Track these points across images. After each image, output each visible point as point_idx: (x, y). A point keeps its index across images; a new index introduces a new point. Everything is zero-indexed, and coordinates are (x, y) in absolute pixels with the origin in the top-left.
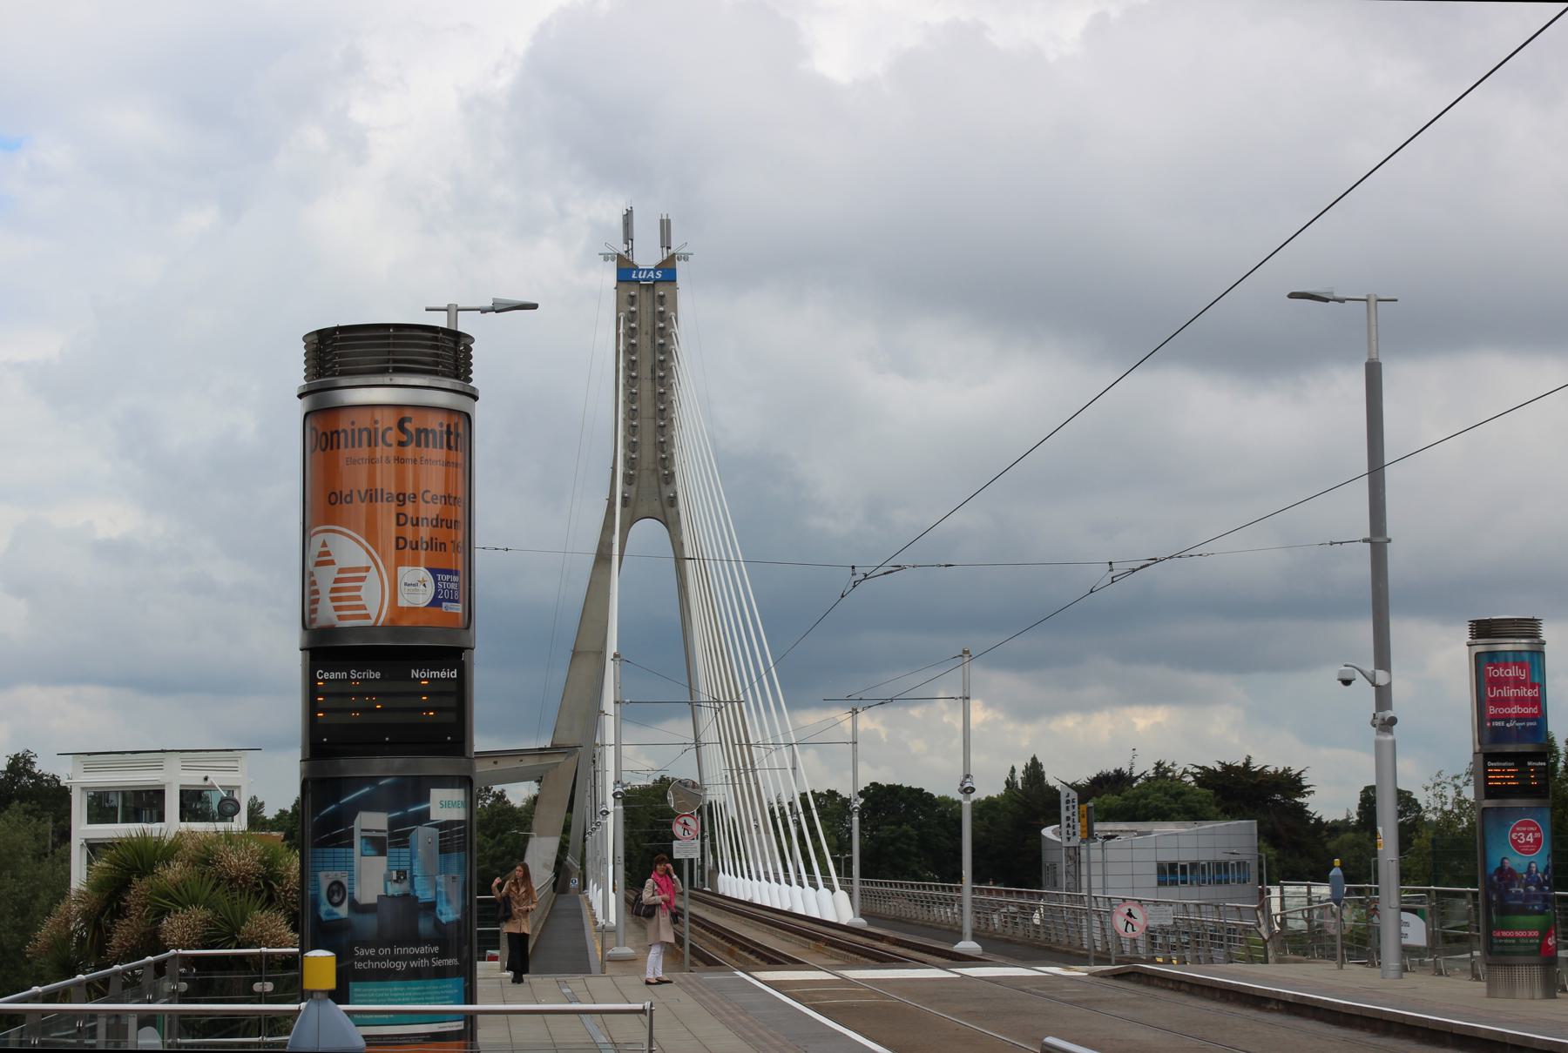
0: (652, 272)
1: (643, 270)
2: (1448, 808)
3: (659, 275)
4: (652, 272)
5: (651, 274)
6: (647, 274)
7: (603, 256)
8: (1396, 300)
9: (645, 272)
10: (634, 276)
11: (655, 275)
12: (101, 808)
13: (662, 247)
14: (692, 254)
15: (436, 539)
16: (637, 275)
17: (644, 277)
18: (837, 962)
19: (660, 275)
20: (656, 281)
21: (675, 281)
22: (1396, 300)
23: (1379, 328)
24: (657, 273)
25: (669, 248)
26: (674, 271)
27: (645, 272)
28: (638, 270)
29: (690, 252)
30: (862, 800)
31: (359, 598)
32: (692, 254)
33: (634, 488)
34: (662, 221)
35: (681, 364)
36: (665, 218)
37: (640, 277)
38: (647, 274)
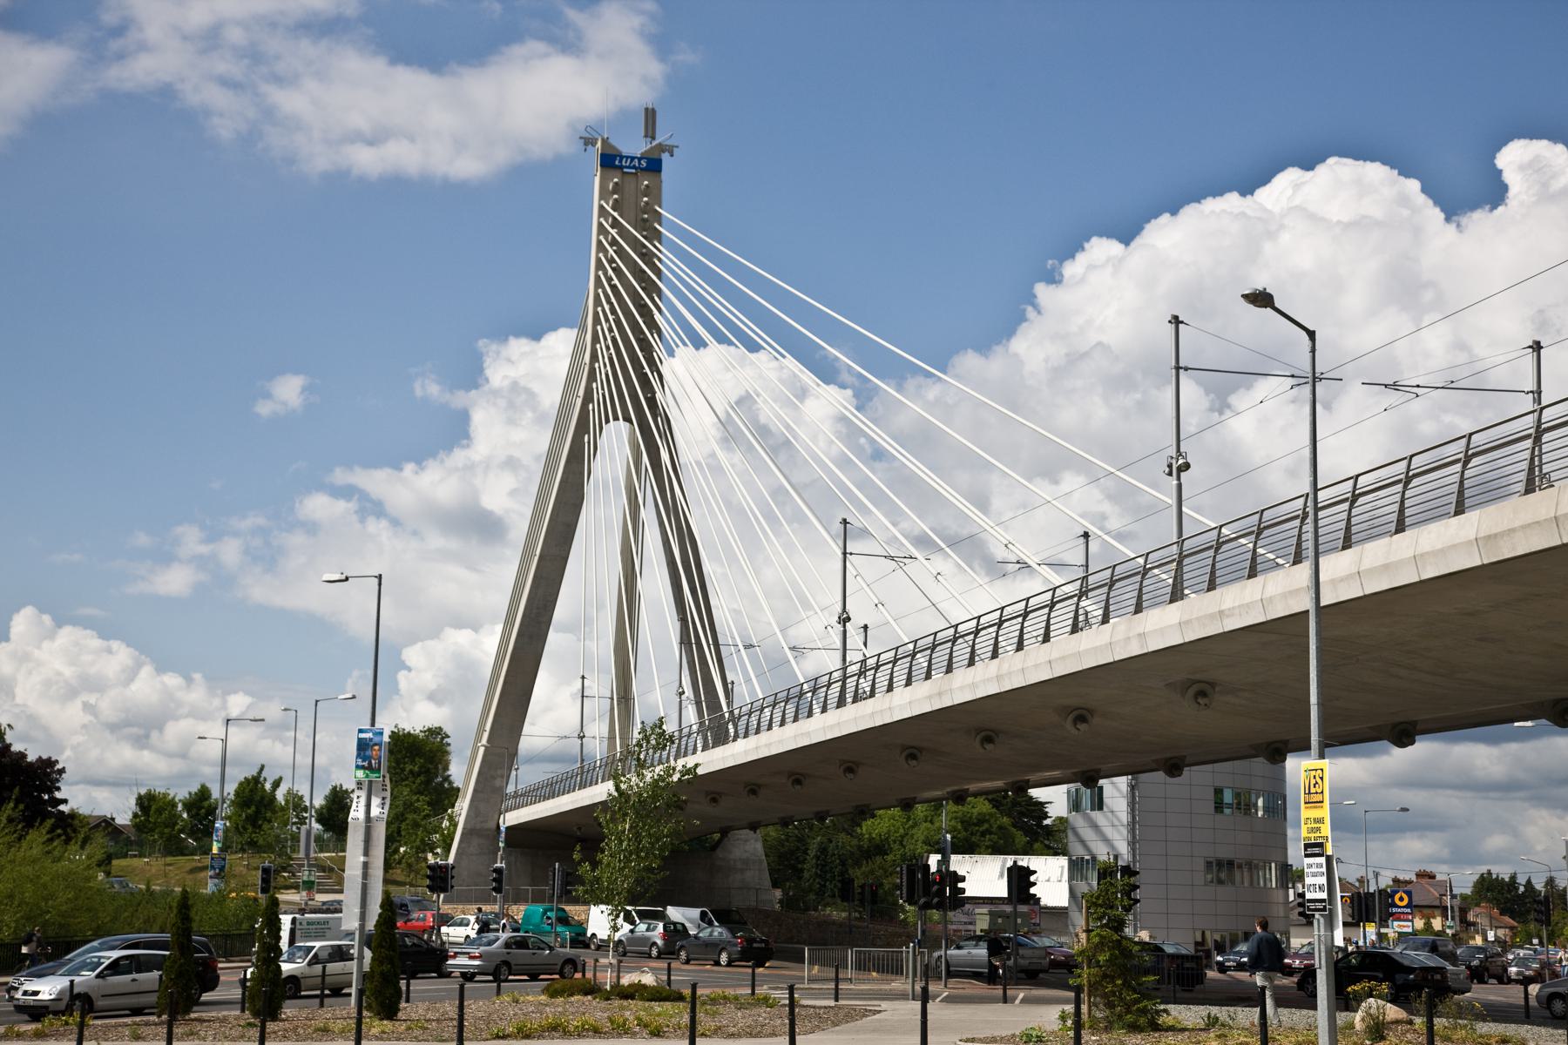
0: (636, 160)
1: (627, 157)
2: (874, 836)
3: (644, 163)
6: (631, 162)
7: (583, 140)
9: (629, 160)
10: (617, 163)
11: (640, 163)
14: (677, 147)
15: (361, 731)
16: (621, 161)
19: (645, 165)
23: (382, 586)
26: (660, 161)
27: (629, 160)
28: (622, 157)
29: (676, 144)
30: (417, 759)
31: (607, 421)
32: (677, 147)
34: (647, 109)
37: (624, 164)
38: (631, 162)
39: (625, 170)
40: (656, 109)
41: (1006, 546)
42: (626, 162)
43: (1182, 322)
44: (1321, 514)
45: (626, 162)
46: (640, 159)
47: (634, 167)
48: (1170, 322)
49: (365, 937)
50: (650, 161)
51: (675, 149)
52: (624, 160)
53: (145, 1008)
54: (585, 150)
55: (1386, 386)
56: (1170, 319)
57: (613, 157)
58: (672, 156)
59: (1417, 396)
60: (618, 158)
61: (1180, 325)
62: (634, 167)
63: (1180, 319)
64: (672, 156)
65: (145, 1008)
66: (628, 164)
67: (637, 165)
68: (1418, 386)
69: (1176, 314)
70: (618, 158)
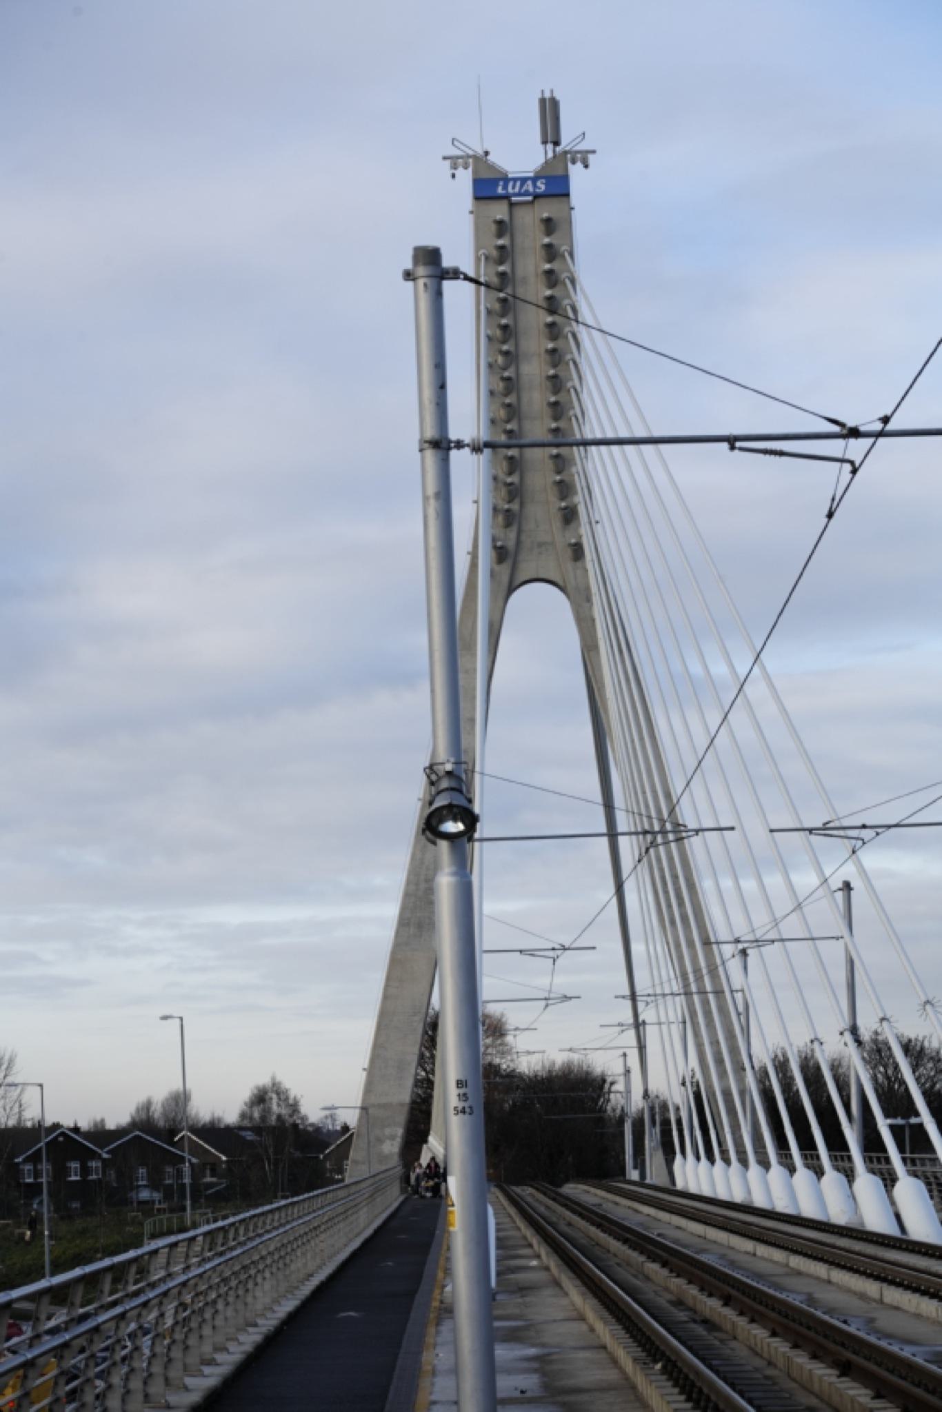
0: (529, 183)
1: (515, 180)
5: (529, 186)
9: (518, 184)
11: (535, 186)
13: (545, 142)
14: (594, 152)
16: (505, 187)
19: (543, 187)
20: (537, 197)
21: (567, 195)
24: (539, 184)
26: (565, 179)
27: (518, 184)
28: (506, 180)
32: (594, 152)
33: (512, 534)
34: (543, 101)
36: (547, 95)
37: (510, 190)
38: (522, 186)
40: (558, 96)
42: (514, 187)
44: (680, 1185)
45: (514, 187)
46: (534, 180)
47: (527, 193)
48: (408, 276)
49: (481, 1069)
50: (550, 180)
51: (591, 157)
53: (831, 507)
54: (453, 176)
55: (521, 951)
56: (409, 265)
57: (494, 182)
58: (586, 166)
59: (864, 843)
60: (501, 183)
61: (447, 285)
62: (527, 193)
63: (447, 262)
64: (586, 166)
65: (831, 507)
66: (517, 190)
67: (531, 189)
68: (864, 827)
69: (430, 242)
70: (501, 183)
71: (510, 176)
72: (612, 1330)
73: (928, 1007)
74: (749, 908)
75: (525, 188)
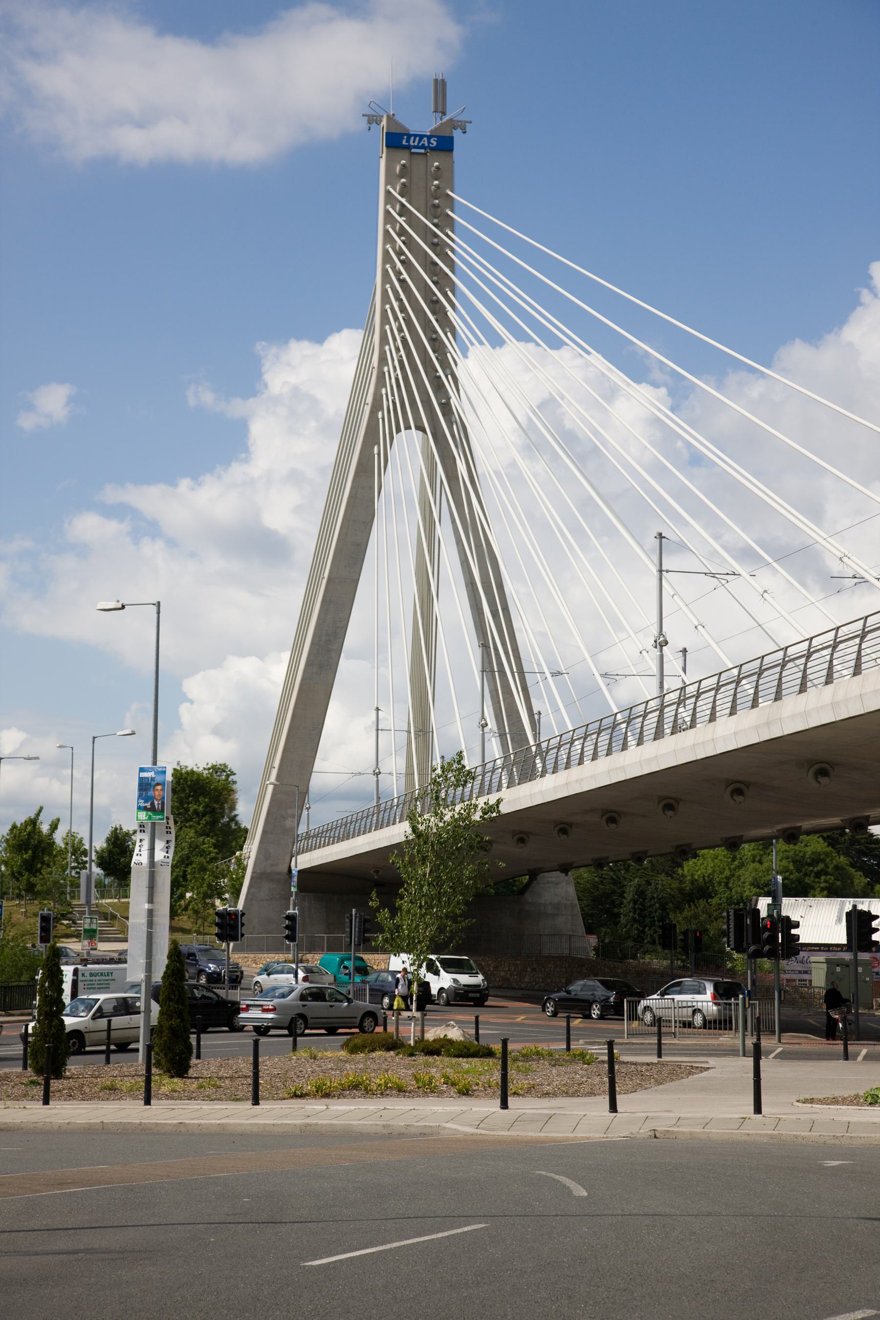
0: (425, 139)
1: (415, 136)
3: (434, 143)
4: (425, 139)
7: (367, 118)
8: (37, 758)
9: (417, 139)
10: (404, 142)
11: (429, 142)
12: (799, 980)
14: (470, 122)
16: (408, 141)
17: (416, 144)
18: (450, 253)
19: (435, 143)
22: (37, 758)
25: (444, 113)
27: (417, 139)
28: (409, 136)
29: (467, 120)
32: (470, 122)
34: (436, 81)
35: (482, 411)
39: (413, 150)
41: (841, 559)
42: (414, 142)
43: (664, 537)
45: (414, 142)
46: (429, 138)
47: (423, 147)
48: (656, 537)
50: (440, 139)
52: (412, 138)
57: (400, 136)
60: (405, 137)
62: (423, 147)
71: (411, 133)
72: (806, 972)
73: (765, 595)
74: (751, 1075)
75: (422, 142)
